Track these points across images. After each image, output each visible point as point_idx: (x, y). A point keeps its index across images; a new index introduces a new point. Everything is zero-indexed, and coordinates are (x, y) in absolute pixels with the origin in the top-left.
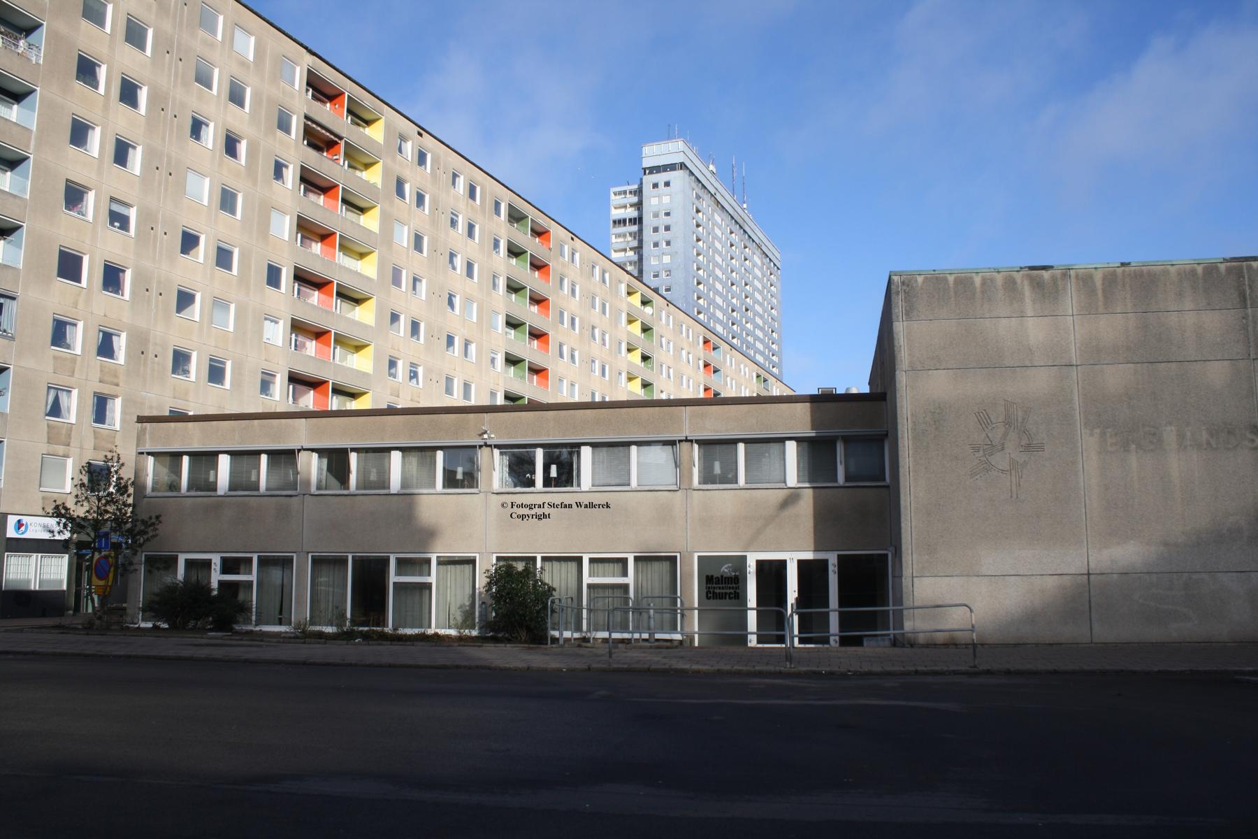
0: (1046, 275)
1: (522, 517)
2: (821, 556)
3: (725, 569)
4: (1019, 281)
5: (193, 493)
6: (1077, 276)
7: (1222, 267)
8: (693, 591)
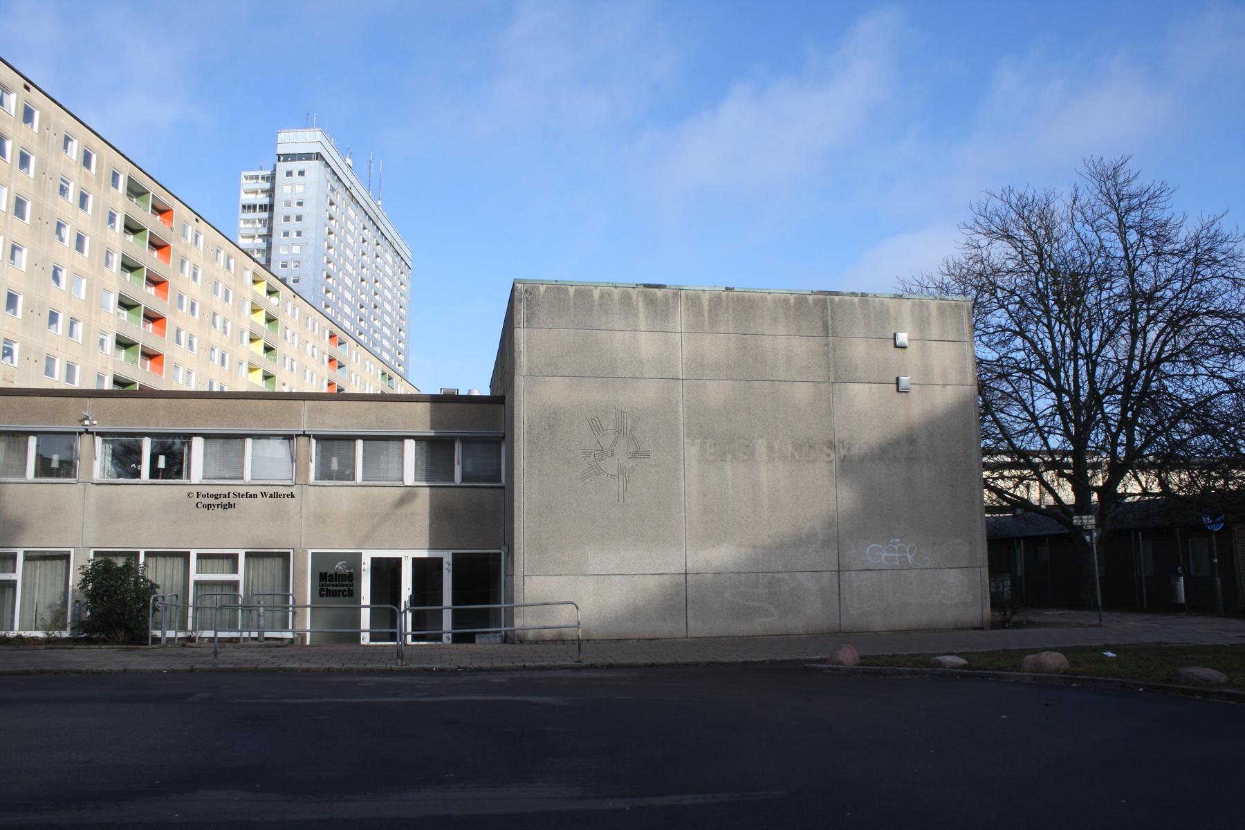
1: (208, 506)
3: (339, 567)
4: (634, 297)
6: (687, 296)
7: (810, 298)
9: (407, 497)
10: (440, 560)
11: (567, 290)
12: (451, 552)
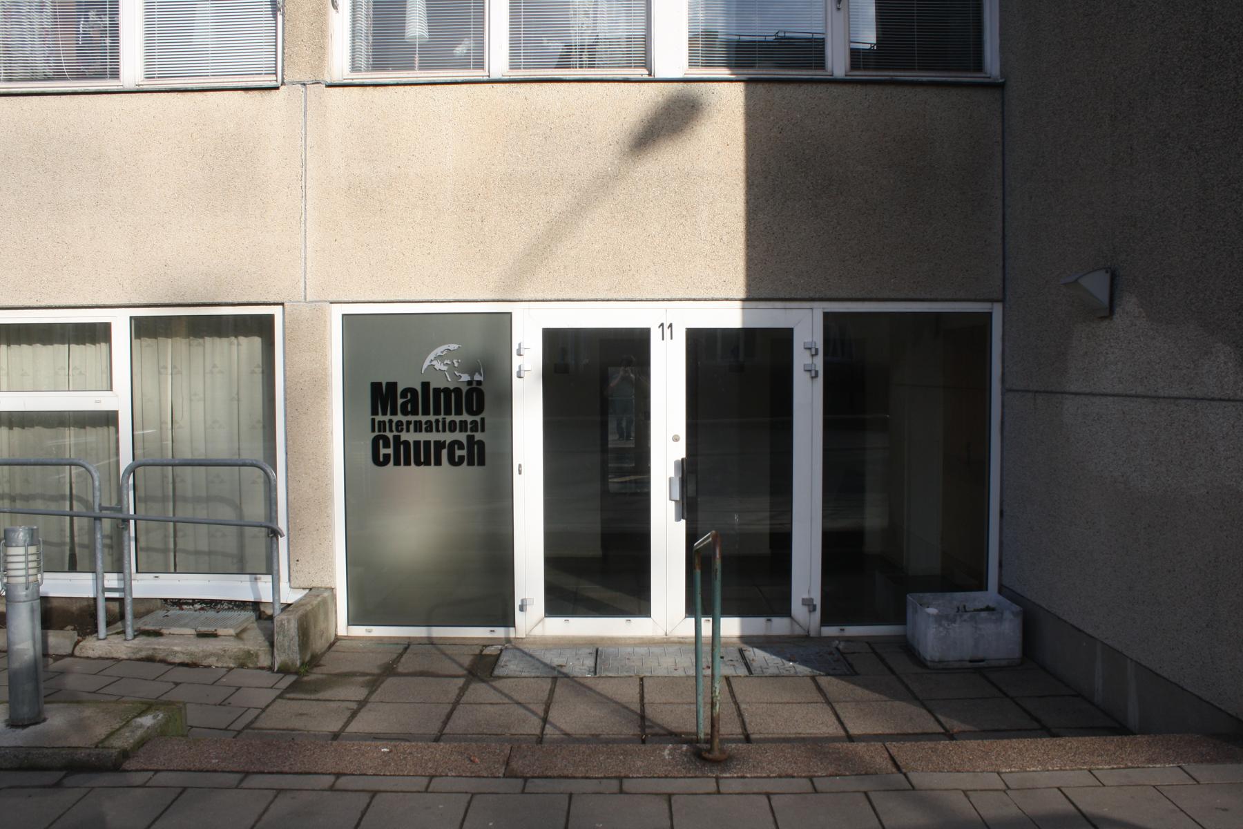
2: (770, 317)
3: (439, 365)
5: (860, 74)
8: (329, 432)
9: (674, 118)
10: (781, 340)
12: (819, 309)
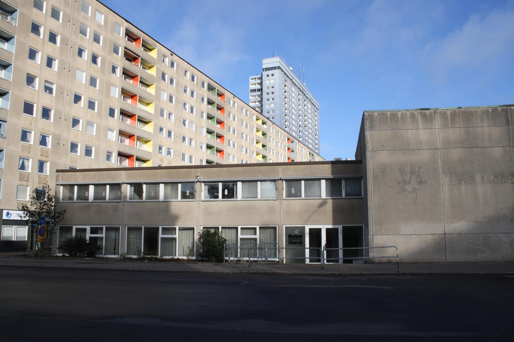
0: (427, 112)
2: (336, 227)
3: (296, 232)
4: (416, 114)
7: (499, 109)
8: (283, 241)
11: (386, 114)
